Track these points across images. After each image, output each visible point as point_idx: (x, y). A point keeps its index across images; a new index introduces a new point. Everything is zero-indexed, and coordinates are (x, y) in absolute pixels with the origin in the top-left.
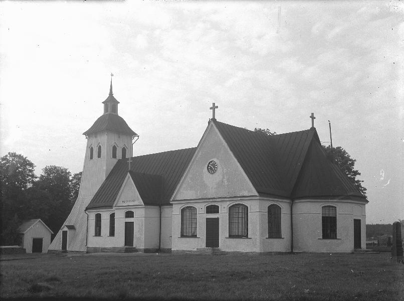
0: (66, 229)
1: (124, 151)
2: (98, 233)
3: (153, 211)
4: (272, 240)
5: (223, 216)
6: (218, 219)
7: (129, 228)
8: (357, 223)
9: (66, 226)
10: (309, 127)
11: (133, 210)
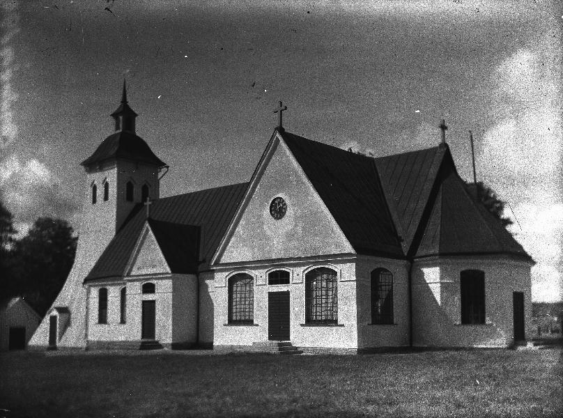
0: (55, 313)
1: (145, 191)
2: (103, 319)
3: (188, 279)
4: (377, 327)
5: (296, 289)
6: (287, 293)
7: (148, 310)
8: (519, 299)
9: (56, 308)
10: (436, 142)
11: (154, 282)
